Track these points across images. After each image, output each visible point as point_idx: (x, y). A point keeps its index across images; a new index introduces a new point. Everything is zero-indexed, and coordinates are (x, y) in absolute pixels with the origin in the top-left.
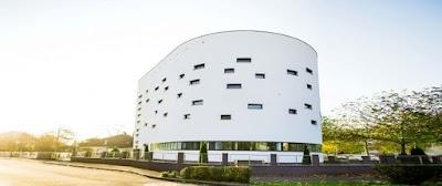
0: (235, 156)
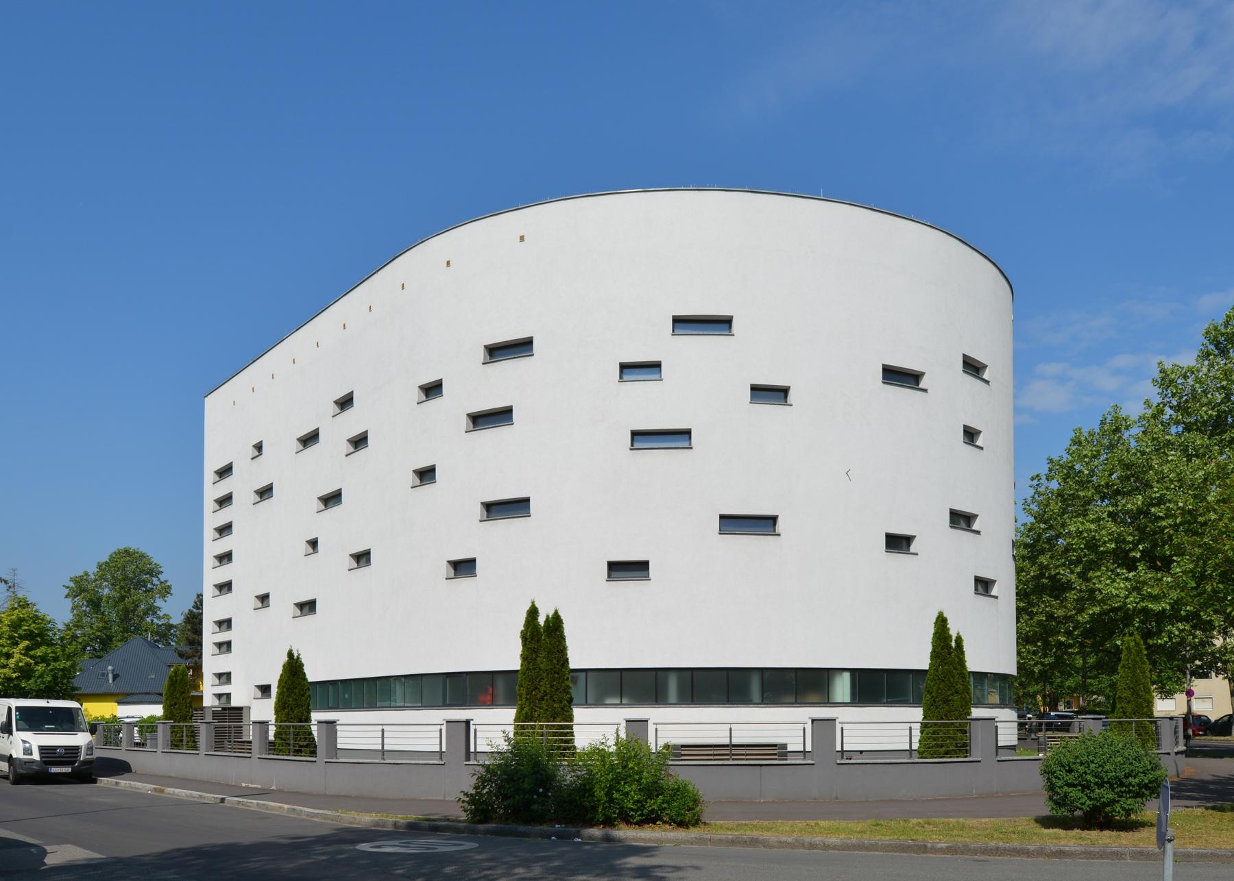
0: (673, 725)
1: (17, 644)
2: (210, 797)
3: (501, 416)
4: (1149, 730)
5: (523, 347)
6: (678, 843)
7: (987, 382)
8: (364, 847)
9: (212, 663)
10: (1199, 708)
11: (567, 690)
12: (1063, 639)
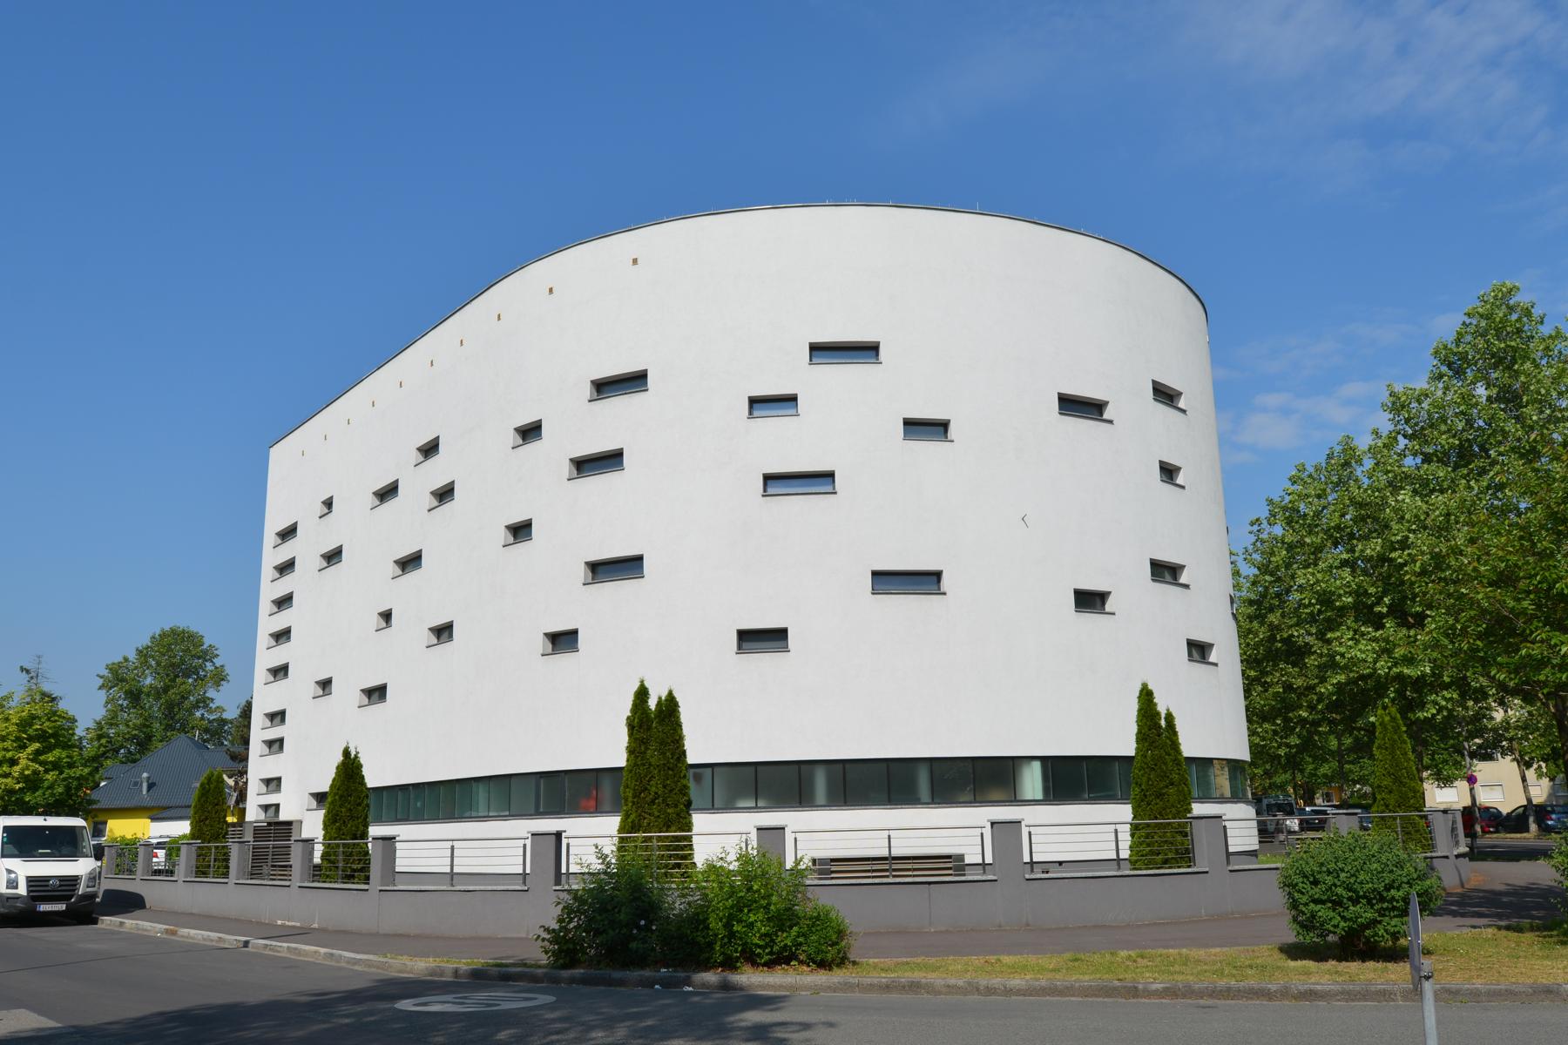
0: (819, 833)
1: (24, 747)
2: (232, 940)
3: (610, 460)
4: (1418, 828)
5: (635, 381)
6: (816, 990)
7: (1184, 411)
8: (406, 1005)
9: (259, 765)
10: (1486, 798)
11: (684, 790)
12: (1305, 714)
